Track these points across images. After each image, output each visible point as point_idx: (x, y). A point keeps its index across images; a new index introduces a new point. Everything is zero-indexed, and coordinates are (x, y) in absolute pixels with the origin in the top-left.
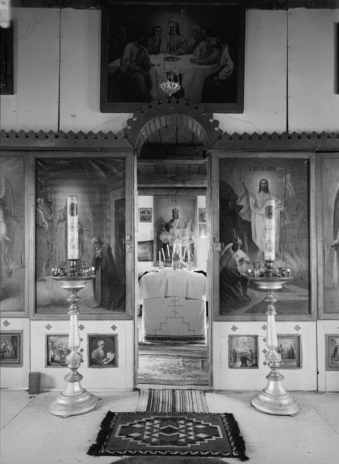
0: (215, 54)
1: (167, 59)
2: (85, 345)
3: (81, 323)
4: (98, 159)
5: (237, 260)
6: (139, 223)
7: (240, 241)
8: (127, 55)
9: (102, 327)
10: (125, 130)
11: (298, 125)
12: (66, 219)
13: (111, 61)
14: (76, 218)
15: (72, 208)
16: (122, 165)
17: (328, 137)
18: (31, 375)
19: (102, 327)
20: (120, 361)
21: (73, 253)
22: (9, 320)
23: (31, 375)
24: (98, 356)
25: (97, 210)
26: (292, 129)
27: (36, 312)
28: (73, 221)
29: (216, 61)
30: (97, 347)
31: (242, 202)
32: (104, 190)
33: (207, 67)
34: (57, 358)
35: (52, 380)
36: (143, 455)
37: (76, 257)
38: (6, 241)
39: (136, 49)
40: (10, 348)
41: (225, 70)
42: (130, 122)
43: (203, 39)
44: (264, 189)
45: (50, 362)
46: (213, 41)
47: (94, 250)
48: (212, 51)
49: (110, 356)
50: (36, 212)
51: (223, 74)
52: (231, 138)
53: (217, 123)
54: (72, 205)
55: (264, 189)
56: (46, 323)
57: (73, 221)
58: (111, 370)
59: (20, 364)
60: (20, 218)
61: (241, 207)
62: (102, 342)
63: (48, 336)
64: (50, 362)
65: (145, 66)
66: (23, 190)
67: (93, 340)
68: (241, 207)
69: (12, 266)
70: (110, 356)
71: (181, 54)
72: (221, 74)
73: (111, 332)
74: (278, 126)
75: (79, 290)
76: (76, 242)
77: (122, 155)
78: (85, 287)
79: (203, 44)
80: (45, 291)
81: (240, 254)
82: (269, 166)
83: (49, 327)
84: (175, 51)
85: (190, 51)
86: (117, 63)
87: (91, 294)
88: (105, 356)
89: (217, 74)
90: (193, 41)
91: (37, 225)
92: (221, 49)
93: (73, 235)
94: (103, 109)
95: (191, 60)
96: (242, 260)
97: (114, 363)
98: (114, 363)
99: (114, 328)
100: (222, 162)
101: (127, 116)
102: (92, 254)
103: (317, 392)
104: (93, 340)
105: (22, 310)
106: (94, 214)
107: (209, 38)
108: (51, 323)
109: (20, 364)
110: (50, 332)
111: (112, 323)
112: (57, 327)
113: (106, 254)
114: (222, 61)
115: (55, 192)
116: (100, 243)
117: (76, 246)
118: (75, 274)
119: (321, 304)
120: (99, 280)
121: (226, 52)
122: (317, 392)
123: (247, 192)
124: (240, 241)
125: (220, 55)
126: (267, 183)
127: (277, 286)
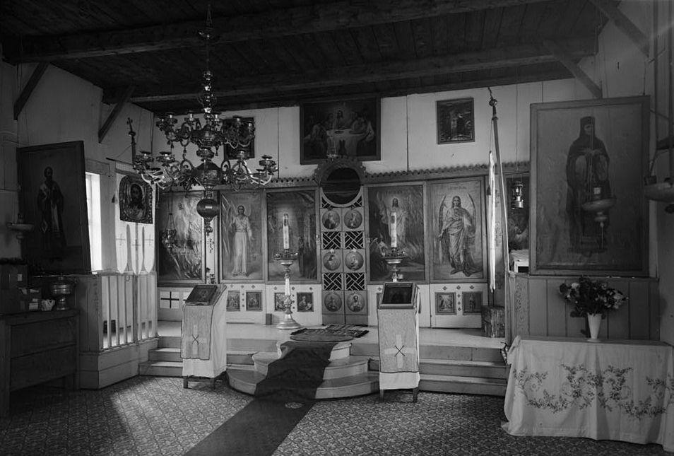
0: (364, 126)
1: (336, 132)
2: (295, 299)
3: (292, 286)
4: (300, 191)
5: (380, 247)
6: (120, 227)
7: (382, 237)
8: (314, 132)
9: (305, 288)
10: (313, 176)
11: (415, 166)
12: (282, 227)
13: (305, 136)
14: (287, 227)
15: (285, 222)
16: (312, 194)
17: (431, 172)
18: (267, 315)
19: (305, 288)
20: (315, 309)
21: (286, 246)
22: (254, 285)
23: (267, 315)
24: (303, 305)
25: (300, 221)
26: (412, 168)
27: (269, 280)
28: (286, 228)
29: (364, 131)
30: (302, 300)
31: (383, 213)
32: (304, 209)
33: (358, 135)
34: (281, 306)
35: (278, 318)
36: (191, 164)
37: (288, 248)
38: (252, 241)
39: (319, 128)
40: (255, 301)
41: (369, 136)
42: (316, 171)
43: (357, 119)
44: (395, 204)
45: (277, 309)
46: (363, 120)
47: (299, 244)
48: (361, 126)
49: (309, 305)
50: (268, 223)
51: (368, 139)
52: (372, 177)
53: (365, 168)
54: (285, 220)
55: (395, 204)
56: (274, 286)
57: (286, 228)
58: (309, 313)
59: (261, 309)
60: (260, 228)
61: (382, 216)
62: (304, 297)
63: (276, 294)
64: (277, 309)
65: (324, 137)
66: (260, 211)
67: (300, 296)
68: (382, 216)
69: (256, 254)
70: (309, 305)
71: (344, 129)
72: (367, 138)
73: (308, 291)
74: (401, 167)
75: (99, 136)
76: (288, 240)
77: (313, 189)
78: (295, 266)
79: (356, 122)
80: (273, 268)
81: (382, 244)
82: (399, 191)
83: (276, 288)
84: (340, 127)
85: (349, 127)
86: (309, 137)
87: (298, 269)
88: (307, 305)
89: (365, 138)
90: (350, 121)
91: (268, 230)
92: (366, 124)
93: (286, 236)
94: (301, 164)
95: (350, 132)
96: (383, 248)
97: (311, 309)
98: (311, 309)
99: (311, 289)
100: (370, 190)
101: (315, 167)
102: (298, 247)
103: (430, 328)
104: (300, 296)
105: (261, 279)
106: (298, 223)
107: (359, 118)
108: (277, 286)
109: (261, 309)
110: (276, 291)
111: (310, 286)
112: (280, 288)
113: (305, 245)
114: (368, 131)
115: (277, 212)
116: (302, 239)
117: (288, 241)
118: (287, 257)
119: (432, 274)
120: (302, 260)
121: (370, 126)
122: (430, 328)
123: (385, 207)
124: (382, 237)
125: (366, 128)
126: (397, 201)
127: (397, 262)
